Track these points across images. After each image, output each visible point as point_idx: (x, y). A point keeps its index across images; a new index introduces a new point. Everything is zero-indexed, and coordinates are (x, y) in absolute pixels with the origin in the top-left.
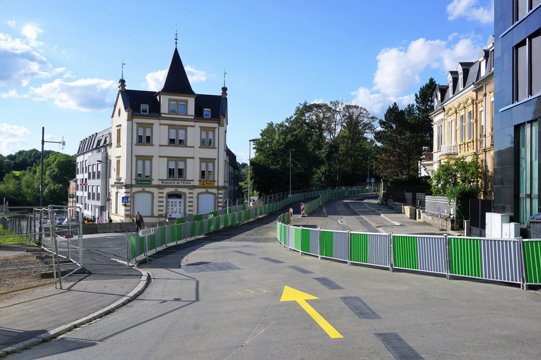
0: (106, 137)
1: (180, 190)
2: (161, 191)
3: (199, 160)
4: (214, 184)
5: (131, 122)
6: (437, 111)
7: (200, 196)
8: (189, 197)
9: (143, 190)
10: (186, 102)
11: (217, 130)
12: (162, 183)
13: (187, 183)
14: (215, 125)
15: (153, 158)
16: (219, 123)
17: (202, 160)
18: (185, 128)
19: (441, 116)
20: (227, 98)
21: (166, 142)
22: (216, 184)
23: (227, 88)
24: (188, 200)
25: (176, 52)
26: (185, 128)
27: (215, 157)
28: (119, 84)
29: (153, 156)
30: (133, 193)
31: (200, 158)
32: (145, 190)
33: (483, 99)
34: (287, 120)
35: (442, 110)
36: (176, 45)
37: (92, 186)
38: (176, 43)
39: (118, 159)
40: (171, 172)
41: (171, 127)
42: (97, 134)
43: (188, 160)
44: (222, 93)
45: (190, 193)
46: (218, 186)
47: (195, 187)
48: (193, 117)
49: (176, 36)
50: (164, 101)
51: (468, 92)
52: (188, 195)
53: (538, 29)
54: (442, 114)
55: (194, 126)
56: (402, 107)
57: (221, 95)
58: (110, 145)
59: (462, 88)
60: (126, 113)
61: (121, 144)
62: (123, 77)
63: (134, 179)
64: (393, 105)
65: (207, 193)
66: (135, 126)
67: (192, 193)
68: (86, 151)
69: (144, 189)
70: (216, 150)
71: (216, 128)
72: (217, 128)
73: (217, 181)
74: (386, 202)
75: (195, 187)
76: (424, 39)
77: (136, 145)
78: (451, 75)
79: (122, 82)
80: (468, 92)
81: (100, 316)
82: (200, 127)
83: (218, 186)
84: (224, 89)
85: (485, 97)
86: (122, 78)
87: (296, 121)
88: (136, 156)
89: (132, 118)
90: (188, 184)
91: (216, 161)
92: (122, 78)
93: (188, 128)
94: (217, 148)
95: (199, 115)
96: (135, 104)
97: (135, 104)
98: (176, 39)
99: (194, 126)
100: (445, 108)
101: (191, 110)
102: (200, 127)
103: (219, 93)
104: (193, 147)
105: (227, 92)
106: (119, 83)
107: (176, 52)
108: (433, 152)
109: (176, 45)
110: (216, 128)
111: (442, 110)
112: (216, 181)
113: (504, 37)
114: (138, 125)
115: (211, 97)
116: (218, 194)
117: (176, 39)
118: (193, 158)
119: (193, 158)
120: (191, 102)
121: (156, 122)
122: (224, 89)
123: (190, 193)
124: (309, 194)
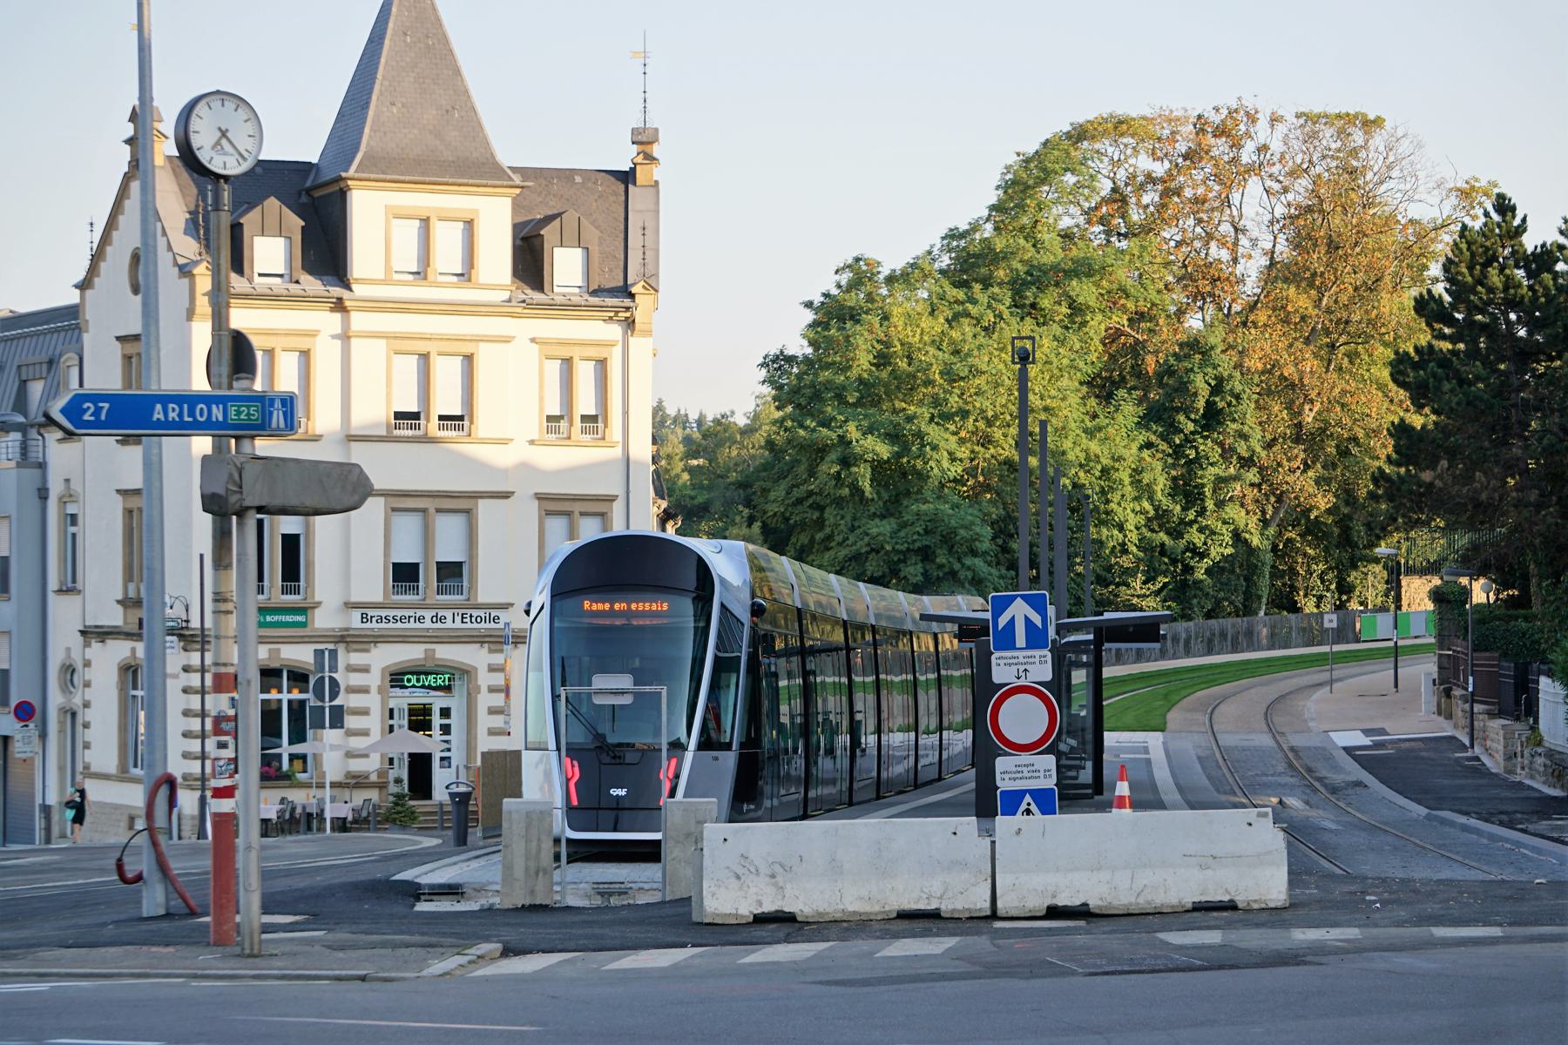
0: (25, 381)
2: (498, 659)
8: (364, 690)
12: (365, 618)
13: (479, 620)
24: (485, 700)
40: (405, 574)
52: (485, 679)
69: (278, 650)
90: (488, 625)
122: (644, 140)
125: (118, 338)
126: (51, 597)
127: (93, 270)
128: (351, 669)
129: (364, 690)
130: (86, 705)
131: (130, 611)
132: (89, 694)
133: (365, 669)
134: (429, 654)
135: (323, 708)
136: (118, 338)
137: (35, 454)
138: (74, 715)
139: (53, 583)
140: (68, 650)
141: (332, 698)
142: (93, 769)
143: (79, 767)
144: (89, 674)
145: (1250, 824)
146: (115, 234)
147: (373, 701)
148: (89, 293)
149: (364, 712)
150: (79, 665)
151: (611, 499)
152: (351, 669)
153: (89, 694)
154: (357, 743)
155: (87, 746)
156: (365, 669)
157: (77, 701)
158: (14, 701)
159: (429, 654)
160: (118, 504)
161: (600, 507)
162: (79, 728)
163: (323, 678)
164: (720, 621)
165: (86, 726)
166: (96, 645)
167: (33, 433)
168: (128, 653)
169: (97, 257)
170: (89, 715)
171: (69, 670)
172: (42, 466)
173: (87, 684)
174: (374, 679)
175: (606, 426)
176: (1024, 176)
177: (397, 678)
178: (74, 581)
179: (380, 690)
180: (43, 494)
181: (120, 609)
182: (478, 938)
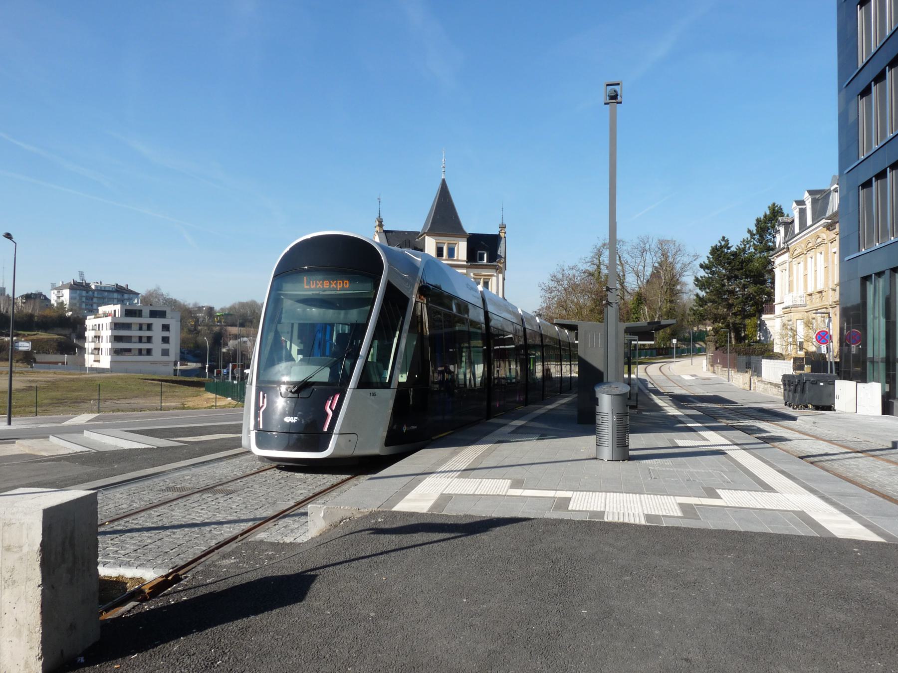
6: (779, 251)
19: (785, 257)
25: (444, 180)
33: (835, 238)
35: (785, 250)
48: (465, 263)
51: (817, 228)
53: (868, 178)
54: (787, 255)
56: (735, 244)
62: (381, 215)
64: (708, 257)
74: (712, 368)
76: (598, 389)
78: (810, 195)
80: (817, 228)
81: (859, 234)
84: (503, 227)
86: (379, 217)
95: (473, 256)
100: (789, 246)
108: (774, 304)
111: (785, 250)
113: (849, 173)
122: (503, 227)
124: (642, 387)
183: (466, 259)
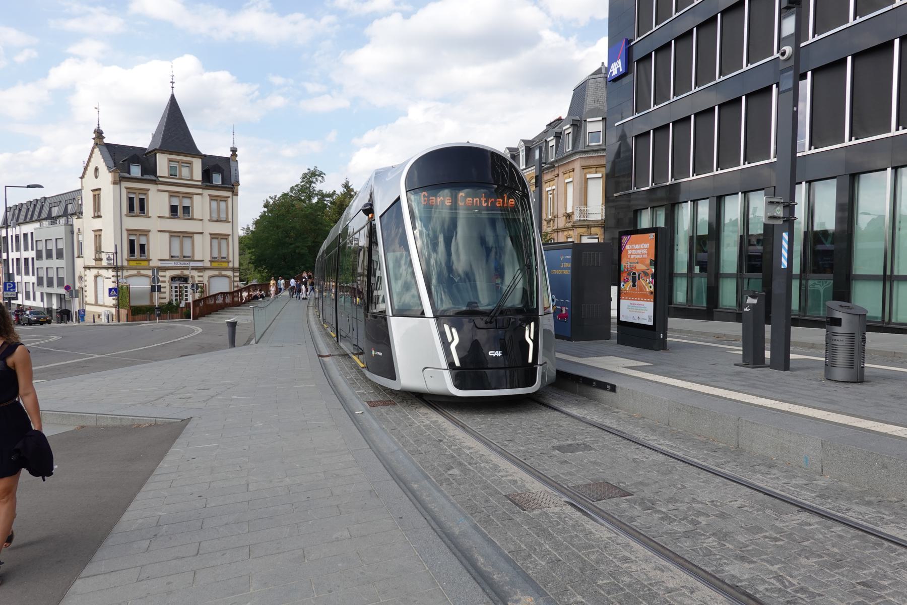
0: (67, 204)
1: (186, 272)
2: (201, 274)
3: (209, 235)
4: (228, 265)
5: (118, 186)
7: (212, 280)
8: (165, 282)
9: (139, 273)
10: (190, 163)
11: (230, 200)
14: (228, 194)
15: (150, 234)
16: (233, 192)
17: (131, 233)
18: (189, 196)
20: (237, 161)
21: (166, 212)
22: (231, 265)
23: (237, 148)
26: (189, 196)
27: (229, 232)
28: (94, 136)
29: (149, 231)
30: (125, 276)
31: (211, 234)
32: (141, 273)
34: (292, 188)
36: (173, 89)
37: (45, 269)
38: (173, 87)
39: (98, 233)
41: (172, 194)
42: (45, 198)
43: (196, 236)
44: (104, 138)
45: (199, 276)
46: (233, 267)
47: (204, 269)
48: (200, 183)
49: (172, 79)
50: (162, 163)
55: (201, 194)
57: (229, 156)
58: (79, 214)
59: (524, 167)
60: (111, 174)
61: (103, 212)
62: (100, 126)
63: (126, 259)
65: (139, 276)
66: (124, 192)
67: (202, 276)
68: (31, 220)
69: (140, 272)
70: (231, 224)
71: (228, 197)
72: (231, 197)
73: (232, 262)
75: (204, 269)
77: (127, 216)
79: (99, 134)
82: (210, 196)
83: (233, 267)
84: (234, 151)
85: (557, 178)
87: (303, 189)
88: (128, 230)
89: (120, 181)
90: (184, 265)
91: (230, 238)
92: (99, 128)
93: (195, 196)
94: (232, 222)
96: (121, 162)
97: (121, 162)
98: (172, 83)
99: (201, 194)
101: (198, 174)
102: (210, 196)
103: (228, 154)
104: (201, 220)
105: (237, 153)
106: (94, 133)
107: (173, 97)
109: (173, 89)
110: (228, 197)
112: (231, 261)
114: (129, 191)
115: (131, 148)
116: (234, 276)
117: (172, 83)
118: (202, 233)
119: (202, 233)
120: (197, 165)
121: (152, 188)
122: (234, 151)
123: (199, 276)
125: (92, 190)
126: (75, 258)
127: (84, 173)
128: (162, 276)
129: (165, 282)
130: (85, 286)
131: (97, 262)
132: (86, 283)
133: (164, 276)
134: (182, 273)
135: (155, 286)
136: (92, 190)
137: (70, 222)
138: (82, 289)
139: (76, 255)
140: (81, 272)
141: (158, 283)
142: (88, 302)
143: (84, 302)
144: (86, 278)
145: (432, 377)
146: (90, 163)
147: (167, 285)
148: (83, 179)
149: (165, 287)
150: (83, 276)
151: (229, 235)
152: (162, 276)
153: (86, 283)
154: (162, 295)
155: (86, 297)
156: (164, 276)
157: (83, 285)
158: (65, 285)
159: (182, 273)
160: (93, 234)
161: (226, 237)
162: (84, 292)
163: (155, 277)
164: (16, 245)
165: (86, 291)
166: (88, 271)
167: (69, 217)
168: (96, 272)
169: (86, 169)
170: (86, 289)
171: (81, 278)
172: (72, 225)
173: (86, 281)
174: (167, 279)
175: (380, 284)
176: (391, 409)
177: (173, 279)
178: (82, 254)
179: (169, 282)
180: (72, 232)
181: (94, 261)
182: (152, 360)
183: (201, 180)
